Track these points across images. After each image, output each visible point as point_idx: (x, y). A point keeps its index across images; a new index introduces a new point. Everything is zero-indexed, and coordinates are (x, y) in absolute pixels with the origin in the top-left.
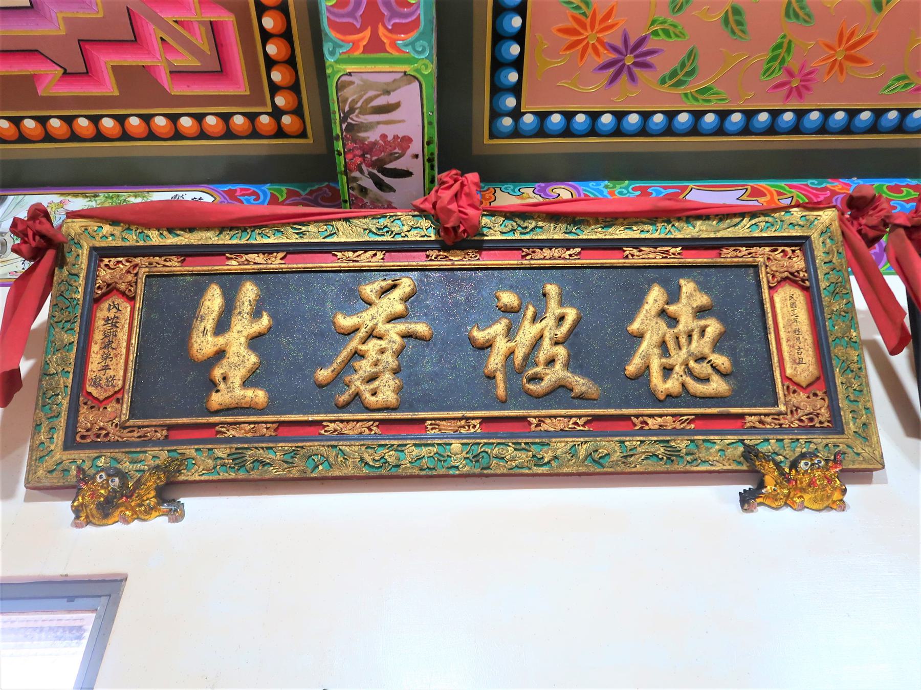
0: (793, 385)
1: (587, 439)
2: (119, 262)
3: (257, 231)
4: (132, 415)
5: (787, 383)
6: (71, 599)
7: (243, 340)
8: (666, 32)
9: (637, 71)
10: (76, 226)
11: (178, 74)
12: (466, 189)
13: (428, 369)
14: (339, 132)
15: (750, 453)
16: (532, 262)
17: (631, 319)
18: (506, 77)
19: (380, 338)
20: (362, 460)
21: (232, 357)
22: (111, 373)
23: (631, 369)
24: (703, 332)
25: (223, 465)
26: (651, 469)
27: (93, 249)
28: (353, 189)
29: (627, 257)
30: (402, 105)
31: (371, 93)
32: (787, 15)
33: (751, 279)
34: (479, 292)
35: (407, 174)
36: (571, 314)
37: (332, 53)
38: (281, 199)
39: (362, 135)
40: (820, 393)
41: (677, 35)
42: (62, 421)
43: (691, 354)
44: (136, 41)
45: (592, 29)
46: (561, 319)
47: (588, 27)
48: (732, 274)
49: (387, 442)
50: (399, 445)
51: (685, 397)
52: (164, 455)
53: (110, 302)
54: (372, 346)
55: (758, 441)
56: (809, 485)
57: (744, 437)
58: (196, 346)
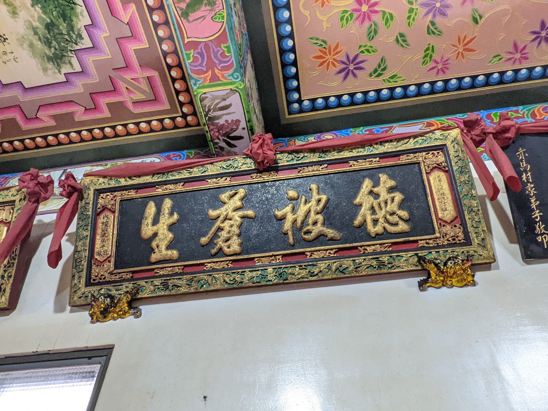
0: (443, 222)
1: (336, 260)
2: (107, 195)
3: (170, 174)
4: (116, 267)
5: (439, 222)
6: (90, 358)
7: (165, 227)
8: (368, 51)
9: (356, 72)
10: (88, 180)
11: (135, 103)
12: (266, 142)
13: (255, 232)
14: (205, 122)
15: (421, 259)
16: (303, 174)
17: (355, 196)
18: (292, 84)
19: (230, 220)
20: (224, 281)
21: (160, 236)
22: (105, 248)
23: (357, 222)
24: (393, 200)
25: (158, 289)
26: (370, 273)
27: (96, 190)
28: (216, 148)
29: (351, 166)
30: (233, 104)
31: (217, 101)
32: (429, 33)
33: (416, 169)
34: (278, 192)
35: (241, 138)
36: (324, 198)
37: (195, 84)
38: (191, 157)
39: (216, 121)
40: (457, 225)
41: (373, 51)
42: (84, 274)
43: (387, 212)
44: (115, 90)
45: (330, 55)
46: (319, 201)
47: (328, 54)
48: (406, 169)
49: (236, 271)
50: (242, 272)
51: (386, 234)
52: (131, 286)
53: (104, 214)
54: (227, 224)
55: (426, 254)
56: (454, 274)
57: (418, 252)
58: (144, 232)
